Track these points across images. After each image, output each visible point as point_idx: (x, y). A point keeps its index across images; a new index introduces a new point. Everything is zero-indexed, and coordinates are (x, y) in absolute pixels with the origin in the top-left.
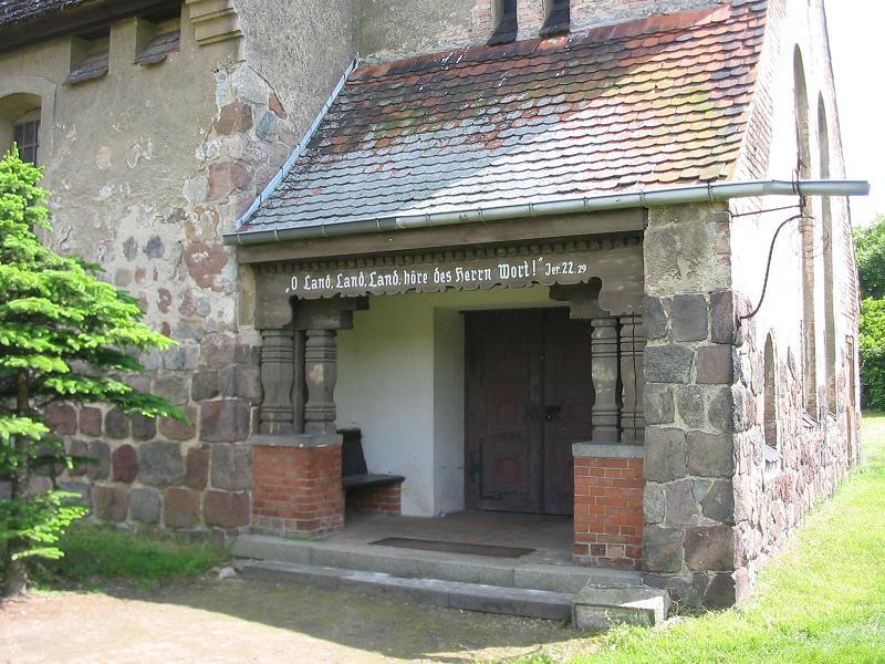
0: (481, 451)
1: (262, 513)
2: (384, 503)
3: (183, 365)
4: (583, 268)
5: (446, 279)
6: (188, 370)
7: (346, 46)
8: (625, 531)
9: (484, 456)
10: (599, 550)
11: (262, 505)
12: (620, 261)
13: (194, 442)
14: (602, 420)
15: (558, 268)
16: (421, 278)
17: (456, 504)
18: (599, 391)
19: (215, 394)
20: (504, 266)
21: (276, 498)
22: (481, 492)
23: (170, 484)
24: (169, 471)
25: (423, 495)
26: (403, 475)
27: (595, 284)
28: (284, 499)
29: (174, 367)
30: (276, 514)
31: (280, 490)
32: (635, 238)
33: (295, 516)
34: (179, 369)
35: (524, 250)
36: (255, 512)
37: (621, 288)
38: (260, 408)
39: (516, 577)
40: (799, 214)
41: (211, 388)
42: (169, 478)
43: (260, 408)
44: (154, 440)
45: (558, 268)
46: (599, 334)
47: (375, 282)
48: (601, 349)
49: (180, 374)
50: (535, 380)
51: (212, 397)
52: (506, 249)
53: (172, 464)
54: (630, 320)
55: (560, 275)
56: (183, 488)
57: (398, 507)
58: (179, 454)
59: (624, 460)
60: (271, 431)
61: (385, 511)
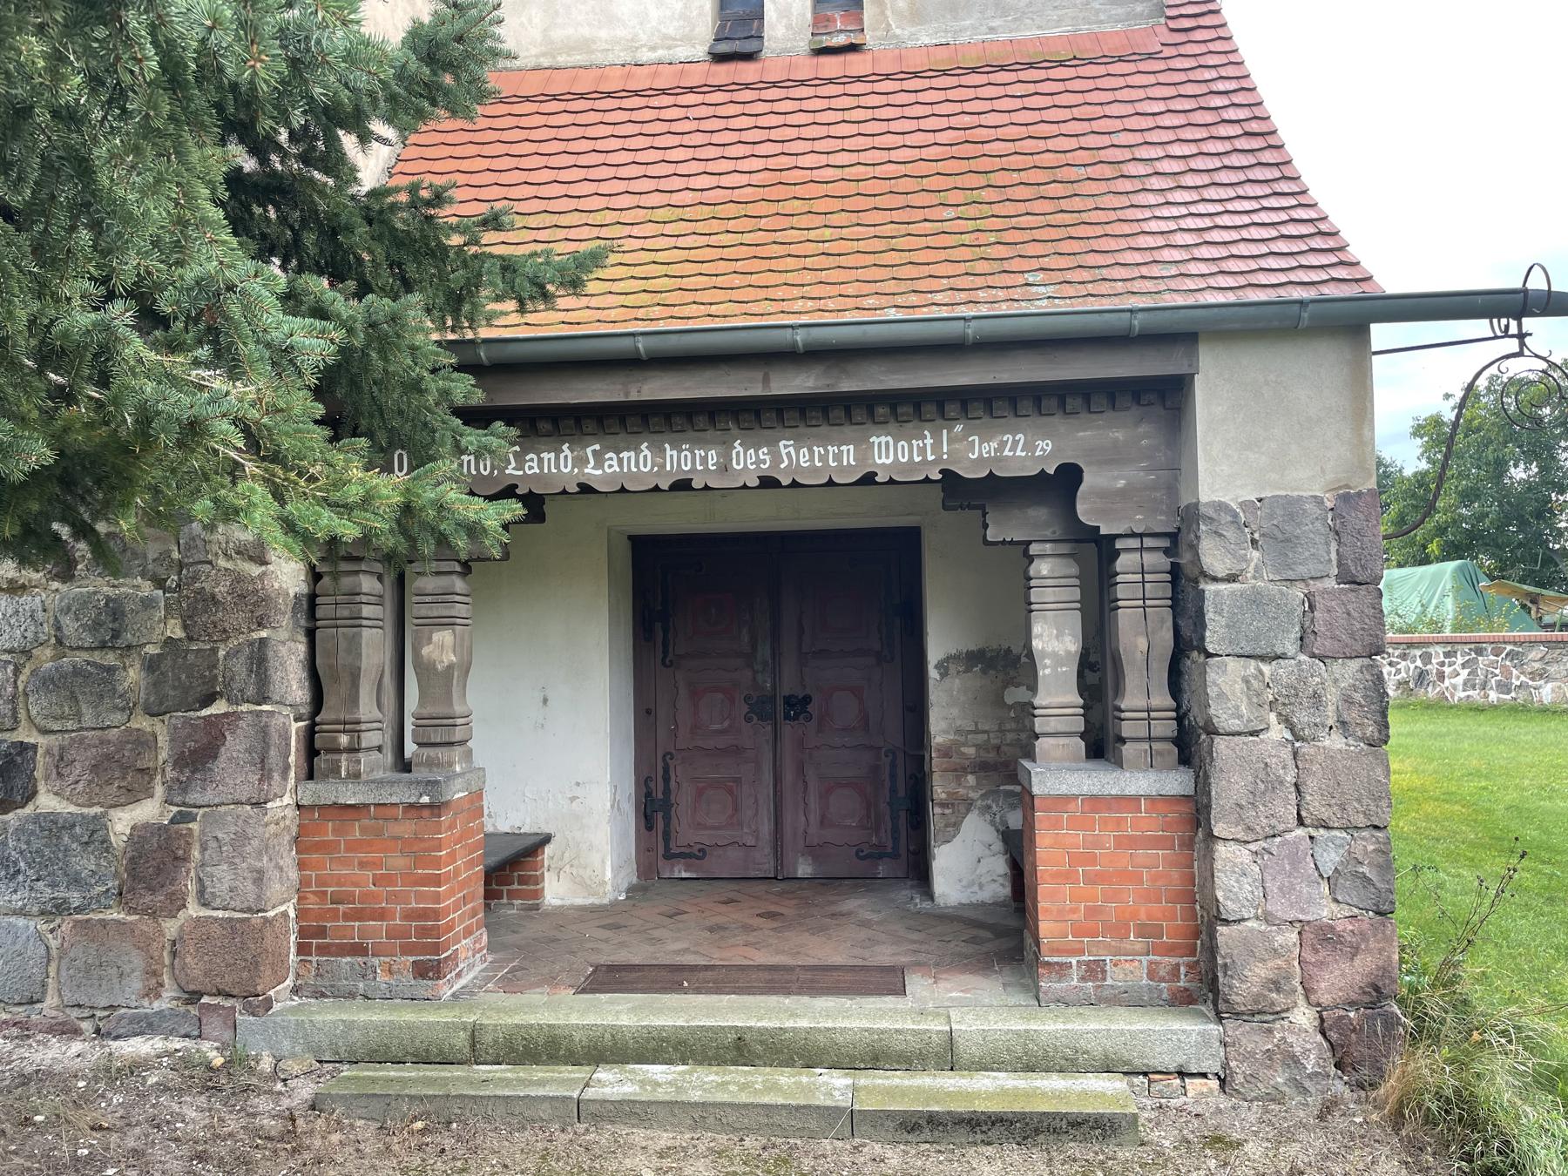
0: (666, 779)
1: (323, 950)
2: (516, 886)
3: (116, 635)
4: (1045, 446)
5: (758, 462)
6: (129, 647)
7: (240, 244)
8: (1142, 932)
9: (673, 784)
10: (1094, 971)
11: (321, 932)
12: (1119, 435)
13: (149, 811)
14: (1053, 725)
15: (994, 445)
16: (704, 460)
17: (630, 876)
18: (1044, 672)
19: (209, 700)
20: (883, 439)
21: (358, 915)
22: (667, 848)
23: (78, 910)
24: (76, 881)
25: (593, 855)
26: (546, 830)
27: (1070, 476)
28: (381, 915)
29: (88, 640)
30: (359, 950)
31: (365, 896)
32: (1168, 399)
33: (407, 950)
34: (103, 646)
35: (929, 409)
36: (302, 949)
37: (1121, 483)
38: (313, 724)
39: (961, 1043)
40: (1517, 350)
41: (200, 690)
42: (75, 898)
43: (313, 724)
44: (28, 810)
45: (994, 445)
46: (1042, 568)
47: (599, 464)
48: (1050, 595)
49: (110, 659)
50: (764, 651)
51: (201, 708)
52: (894, 408)
53: (85, 864)
54: (1134, 543)
55: (999, 460)
56: (115, 915)
57: (538, 894)
58: (106, 840)
59: (1136, 799)
60: (343, 774)
61: (517, 902)
